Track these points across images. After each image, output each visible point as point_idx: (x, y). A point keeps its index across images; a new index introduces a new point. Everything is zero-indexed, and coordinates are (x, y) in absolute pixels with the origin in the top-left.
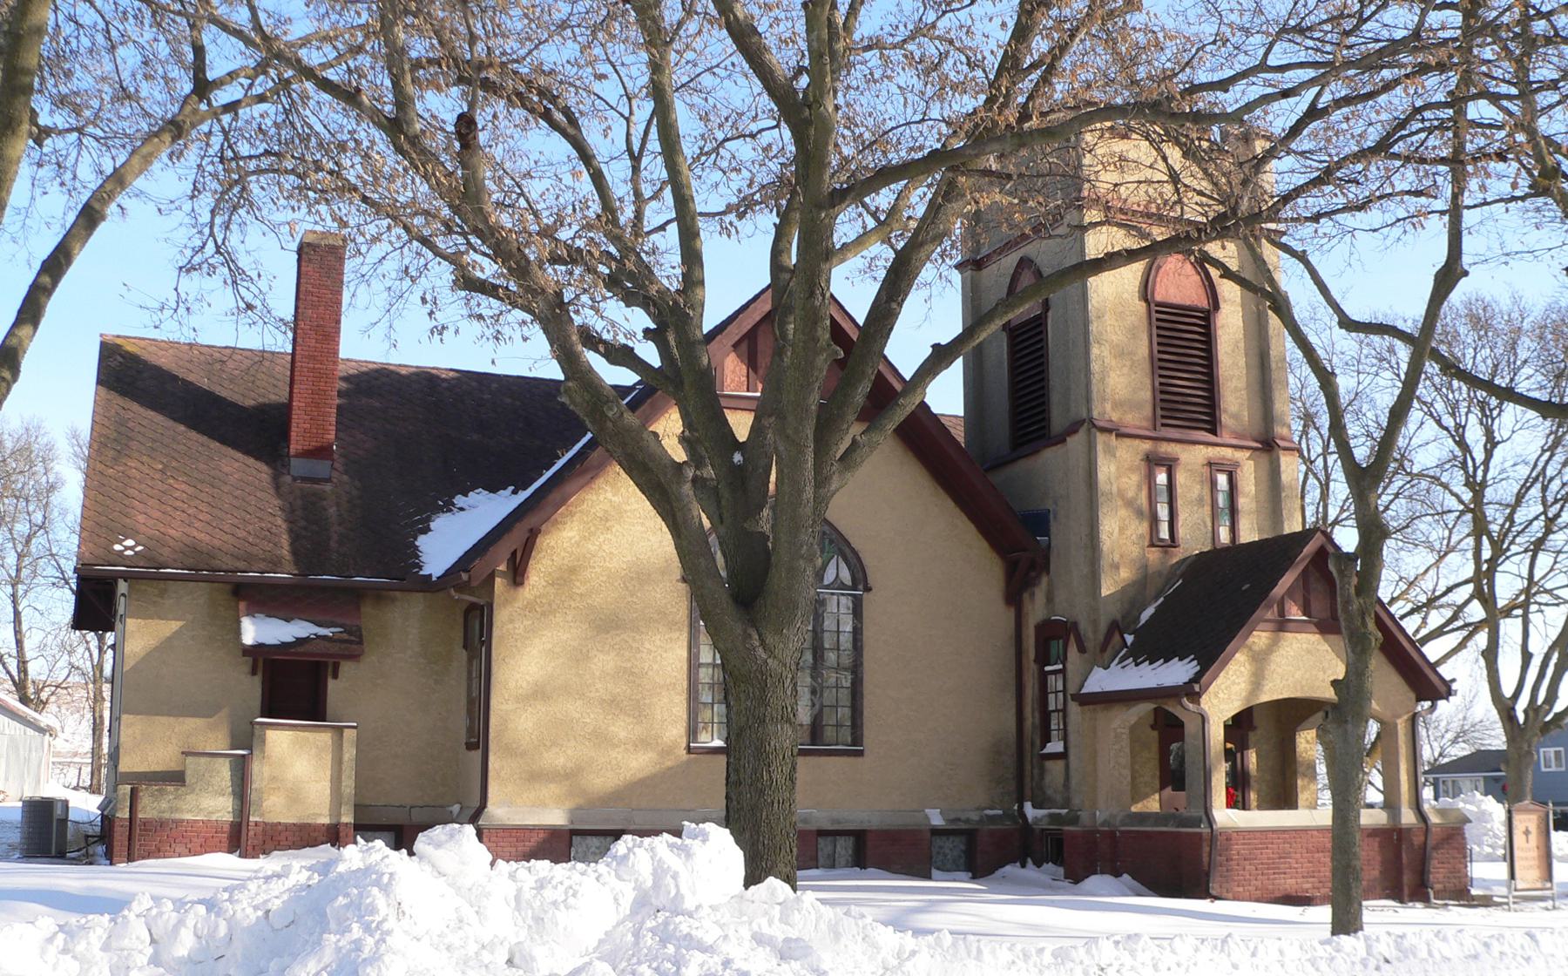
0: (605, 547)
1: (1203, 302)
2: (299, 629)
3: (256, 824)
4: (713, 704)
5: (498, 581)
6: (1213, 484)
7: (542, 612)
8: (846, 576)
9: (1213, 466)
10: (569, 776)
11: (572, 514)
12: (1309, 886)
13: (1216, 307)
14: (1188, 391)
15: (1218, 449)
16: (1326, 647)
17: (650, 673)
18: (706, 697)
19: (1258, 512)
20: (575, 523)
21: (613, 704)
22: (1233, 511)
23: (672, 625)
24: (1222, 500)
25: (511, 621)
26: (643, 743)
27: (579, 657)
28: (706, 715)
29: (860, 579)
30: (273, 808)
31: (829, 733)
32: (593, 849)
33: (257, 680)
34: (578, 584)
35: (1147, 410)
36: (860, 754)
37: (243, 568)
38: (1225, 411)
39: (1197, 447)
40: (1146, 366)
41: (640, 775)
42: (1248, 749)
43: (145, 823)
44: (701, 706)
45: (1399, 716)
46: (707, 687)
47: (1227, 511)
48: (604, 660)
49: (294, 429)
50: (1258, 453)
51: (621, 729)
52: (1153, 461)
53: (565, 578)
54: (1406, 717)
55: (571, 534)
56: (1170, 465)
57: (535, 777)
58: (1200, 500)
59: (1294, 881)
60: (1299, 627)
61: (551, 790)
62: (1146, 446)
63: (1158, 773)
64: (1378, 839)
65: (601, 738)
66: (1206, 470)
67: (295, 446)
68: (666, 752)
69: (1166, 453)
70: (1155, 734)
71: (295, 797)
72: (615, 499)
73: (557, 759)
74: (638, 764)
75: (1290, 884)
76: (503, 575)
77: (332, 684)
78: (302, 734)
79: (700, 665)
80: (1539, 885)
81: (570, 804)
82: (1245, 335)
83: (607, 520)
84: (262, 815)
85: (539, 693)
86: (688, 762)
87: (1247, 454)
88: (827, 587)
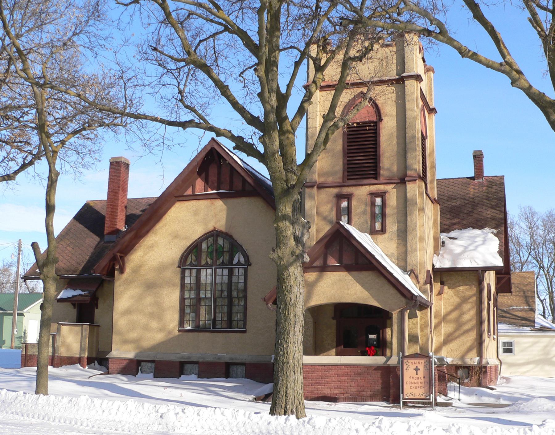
0: (152, 257)
1: (374, 119)
2: (78, 292)
3: (58, 356)
4: (190, 313)
5: (116, 272)
6: (373, 204)
7: (129, 282)
8: (242, 260)
9: (374, 195)
10: (136, 341)
11: (141, 246)
12: (337, 392)
13: (380, 120)
14: (364, 161)
15: (376, 186)
16: (350, 277)
17: (167, 302)
18: (188, 310)
19: (398, 213)
20: (142, 249)
21: (152, 315)
22: (383, 215)
23: (174, 285)
24: (377, 211)
25: (120, 286)
26: (161, 330)
27: (140, 298)
28: (187, 317)
29: (248, 263)
30: (63, 352)
31: (234, 323)
32: (149, 367)
33: (76, 310)
34: (142, 271)
35: (340, 174)
36: (245, 332)
37: (64, 274)
38: (383, 168)
39: (364, 187)
40: (341, 154)
41: (162, 340)
42: (386, 328)
43: (30, 355)
44: (186, 314)
45: (394, 310)
46: (188, 306)
47: (380, 215)
48: (149, 300)
49: (106, 225)
50: (399, 185)
51: (154, 324)
52: (340, 197)
53: (136, 270)
54: (398, 310)
55: (140, 253)
56: (349, 197)
57: (125, 342)
58: (364, 213)
59: (329, 389)
60: (334, 269)
61: (130, 347)
62: (335, 191)
63: (335, 339)
64: (380, 371)
65: (146, 328)
66: (369, 198)
67: (106, 232)
68: (170, 332)
69: (347, 192)
70: (335, 322)
71: (68, 347)
72: (156, 239)
73: (133, 335)
74: (159, 337)
75: (327, 391)
76: (118, 270)
77: (96, 311)
78: (72, 327)
79: (185, 299)
80: (423, 397)
81: (137, 351)
82: (397, 130)
83: (153, 247)
84: (58, 354)
85: (127, 312)
86: (178, 336)
87: (393, 186)
88: (235, 265)
